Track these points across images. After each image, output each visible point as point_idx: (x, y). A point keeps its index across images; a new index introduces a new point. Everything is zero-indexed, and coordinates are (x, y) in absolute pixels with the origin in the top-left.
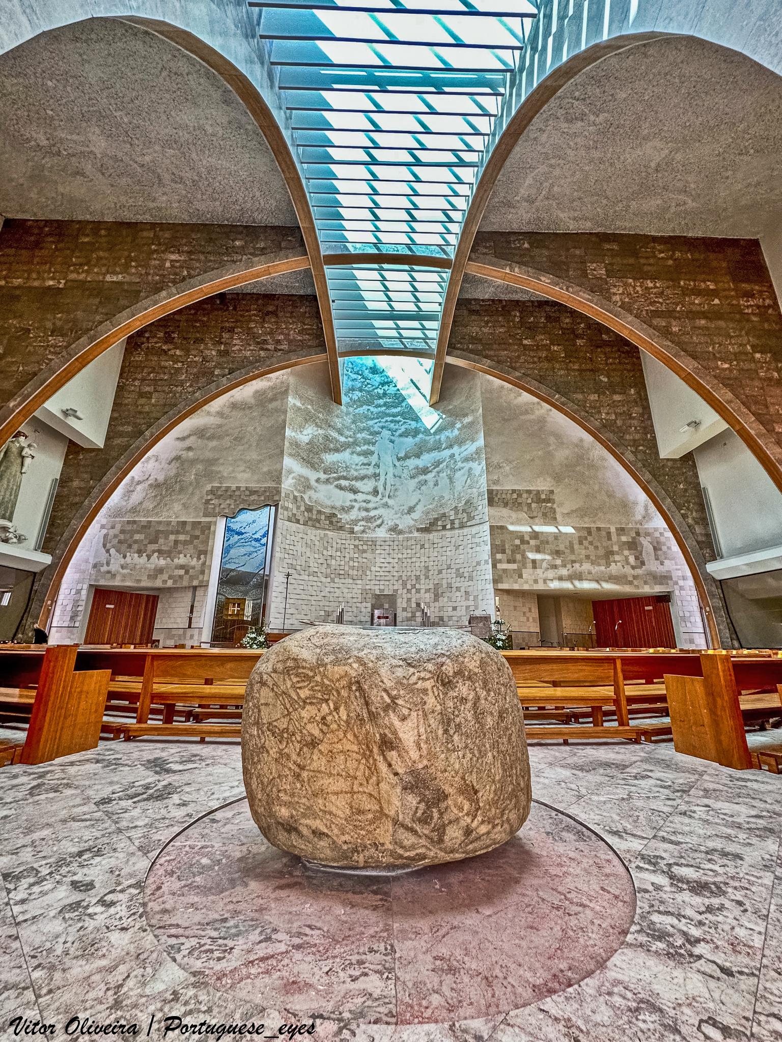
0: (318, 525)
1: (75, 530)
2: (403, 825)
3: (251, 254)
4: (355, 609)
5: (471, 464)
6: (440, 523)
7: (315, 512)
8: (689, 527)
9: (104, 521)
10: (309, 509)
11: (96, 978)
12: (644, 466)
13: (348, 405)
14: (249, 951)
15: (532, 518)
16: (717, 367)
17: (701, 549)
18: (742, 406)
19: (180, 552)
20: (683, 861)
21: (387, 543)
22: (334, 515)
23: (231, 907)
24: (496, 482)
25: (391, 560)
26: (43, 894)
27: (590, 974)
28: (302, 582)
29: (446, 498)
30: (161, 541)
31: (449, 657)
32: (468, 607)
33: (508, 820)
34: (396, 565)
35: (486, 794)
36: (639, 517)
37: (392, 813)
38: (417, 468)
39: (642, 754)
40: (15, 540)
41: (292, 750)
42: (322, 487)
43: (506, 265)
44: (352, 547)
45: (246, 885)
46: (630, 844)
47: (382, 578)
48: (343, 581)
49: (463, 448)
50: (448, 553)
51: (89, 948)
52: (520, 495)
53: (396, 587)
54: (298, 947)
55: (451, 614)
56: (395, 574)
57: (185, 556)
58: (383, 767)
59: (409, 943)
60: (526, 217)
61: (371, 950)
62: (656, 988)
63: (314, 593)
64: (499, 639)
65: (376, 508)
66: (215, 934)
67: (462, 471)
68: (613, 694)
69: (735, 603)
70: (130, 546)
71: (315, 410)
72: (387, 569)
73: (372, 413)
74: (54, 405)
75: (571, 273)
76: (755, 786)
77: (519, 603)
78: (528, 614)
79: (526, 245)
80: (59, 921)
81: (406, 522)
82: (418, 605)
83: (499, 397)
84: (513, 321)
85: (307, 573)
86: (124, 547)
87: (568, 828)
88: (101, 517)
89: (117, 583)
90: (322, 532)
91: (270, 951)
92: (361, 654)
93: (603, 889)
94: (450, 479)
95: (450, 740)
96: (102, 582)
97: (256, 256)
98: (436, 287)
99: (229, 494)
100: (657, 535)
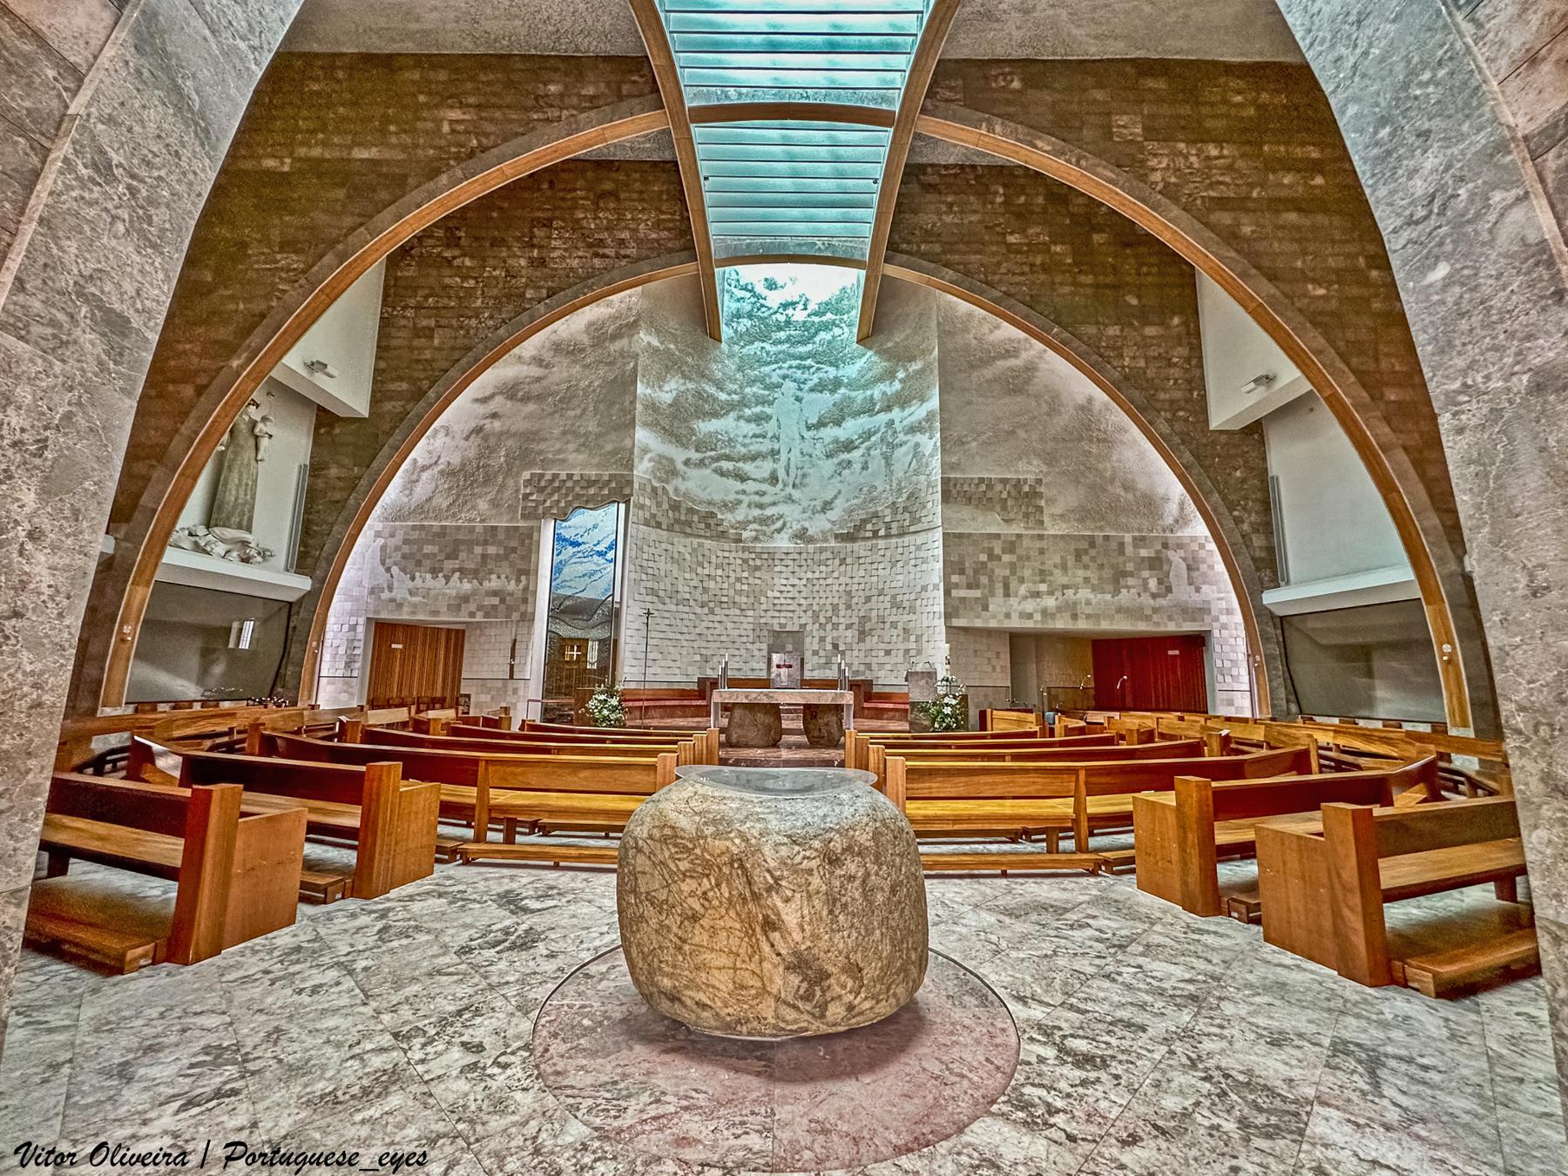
0: (688, 530)
1: (340, 541)
2: (785, 1002)
3: (574, 108)
4: (743, 652)
5: (919, 438)
6: (869, 527)
7: (683, 511)
8: (1243, 536)
9: (379, 526)
10: (675, 507)
11: (513, 1130)
12: (1183, 442)
13: (732, 342)
14: (641, 1111)
16: (1305, 295)
17: (1258, 569)
19: (491, 572)
20: (1081, 1033)
22: (712, 515)
23: (619, 1070)
25: (796, 582)
26: (439, 1054)
27: (947, 1137)
29: (880, 489)
30: (463, 555)
31: (838, 831)
32: (907, 651)
33: (895, 994)
35: (871, 972)
37: (775, 991)
38: (836, 441)
39: (1095, 892)
40: (259, 559)
41: (673, 922)
42: (693, 473)
43: (981, 121)
45: (631, 1049)
46: (1032, 1012)
49: (907, 412)
50: (881, 572)
51: (500, 1105)
52: (990, 486)
53: (803, 621)
54: (686, 1109)
56: (802, 601)
58: (766, 948)
59: (788, 1108)
60: (1017, 35)
61: (753, 1113)
62: (1002, 1150)
65: (774, 504)
66: (608, 1095)
67: (904, 448)
68: (1071, 810)
69: (1298, 647)
74: (293, 360)
76: (1209, 939)
78: (994, 662)
79: (1016, 85)
80: (463, 1081)
81: (819, 525)
82: (835, 646)
84: (992, 203)
87: (973, 992)
88: (374, 523)
89: (405, 616)
91: (660, 1112)
92: (744, 828)
93: (987, 1060)
94: (886, 458)
95: (835, 920)
96: (385, 615)
97: (583, 110)
99: (553, 486)
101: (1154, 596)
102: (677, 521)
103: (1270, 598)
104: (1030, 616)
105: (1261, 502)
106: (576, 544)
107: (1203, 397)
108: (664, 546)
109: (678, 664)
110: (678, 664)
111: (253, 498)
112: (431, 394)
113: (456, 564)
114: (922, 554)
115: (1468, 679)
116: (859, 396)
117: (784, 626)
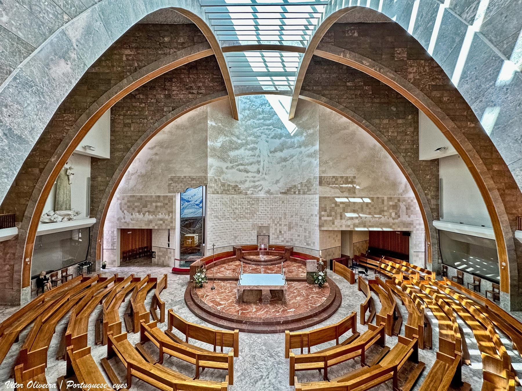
0: (228, 193)
3: (175, 48)
6: (292, 190)
10: (223, 185)
12: (409, 165)
13: (242, 120)
15: (342, 192)
17: (432, 212)
18: (476, 154)
22: (237, 186)
24: (324, 172)
28: (222, 224)
30: (149, 206)
32: (305, 236)
34: (269, 211)
36: (401, 191)
38: (281, 158)
43: (341, 52)
44: (246, 202)
48: (243, 220)
49: (307, 148)
50: (297, 207)
52: (337, 179)
53: (269, 223)
55: (296, 238)
64: (320, 275)
65: (259, 181)
70: (134, 209)
71: (224, 126)
73: (256, 124)
75: (383, 56)
77: (331, 234)
79: (356, 34)
81: (275, 188)
82: (280, 232)
83: (329, 119)
86: (131, 209)
88: (117, 195)
89: (130, 227)
90: (231, 196)
98: (297, 60)
100: (409, 201)
101: (393, 219)
102: (224, 190)
103: (437, 224)
104: (349, 226)
105: (437, 187)
106: (188, 201)
107: (418, 147)
108: (220, 200)
109: (226, 240)
110: (226, 240)
111: (70, 197)
112: (132, 149)
113: (146, 209)
114: (311, 202)
115: (511, 277)
116: (289, 141)
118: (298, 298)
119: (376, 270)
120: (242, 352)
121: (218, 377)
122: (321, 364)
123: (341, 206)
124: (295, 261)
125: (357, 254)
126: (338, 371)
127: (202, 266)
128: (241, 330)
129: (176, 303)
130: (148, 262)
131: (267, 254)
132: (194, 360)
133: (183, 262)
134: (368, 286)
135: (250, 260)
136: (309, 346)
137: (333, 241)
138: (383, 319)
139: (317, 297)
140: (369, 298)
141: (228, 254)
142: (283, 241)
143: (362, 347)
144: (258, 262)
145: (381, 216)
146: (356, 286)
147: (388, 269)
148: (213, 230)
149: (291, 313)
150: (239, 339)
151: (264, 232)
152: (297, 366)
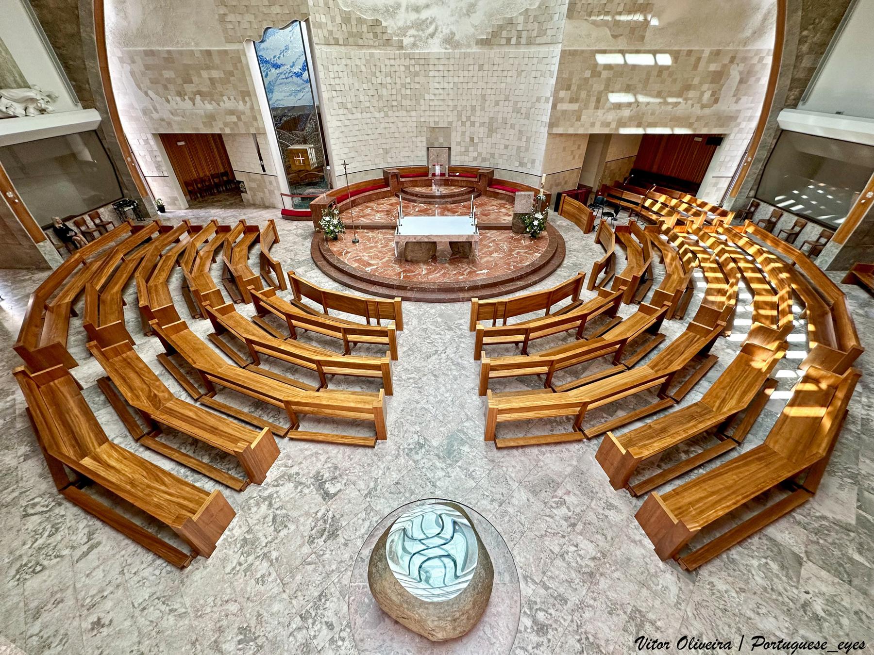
0: (360, 42)
4: (410, 144)
6: (504, 34)
7: (354, 22)
21: (442, 62)
22: (377, 23)
30: (195, 79)
32: (519, 148)
34: (451, 92)
44: (403, 68)
47: (437, 108)
48: (397, 114)
50: (509, 80)
53: (450, 119)
56: (450, 103)
57: (229, 99)
63: (370, 132)
64: (537, 219)
72: (441, 97)
82: (472, 139)
85: (359, 110)
102: (351, 34)
104: (608, 125)
106: (277, 66)
108: (344, 62)
117: (436, 122)
118: (495, 255)
119: (633, 210)
120: (408, 325)
121: (376, 352)
122: (521, 338)
123: (605, 74)
124: (496, 195)
125: (608, 182)
126: (541, 345)
127: (331, 206)
128: (404, 299)
129: (300, 263)
130: (237, 201)
131: (446, 183)
132: (340, 335)
133: (297, 200)
134: (614, 236)
135: (416, 195)
136: (505, 317)
137: (570, 158)
138: (624, 282)
139: (526, 253)
140: (609, 254)
141: (375, 185)
142: (475, 159)
143: (583, 317)
144: (429, 199)
145: (680, 100)
146: (593, 236)
147: (656, 208)
148: (341, 135)
149: (482, 275)
150: (403, 310)
151: (441, 140)
152: (486, 340)
